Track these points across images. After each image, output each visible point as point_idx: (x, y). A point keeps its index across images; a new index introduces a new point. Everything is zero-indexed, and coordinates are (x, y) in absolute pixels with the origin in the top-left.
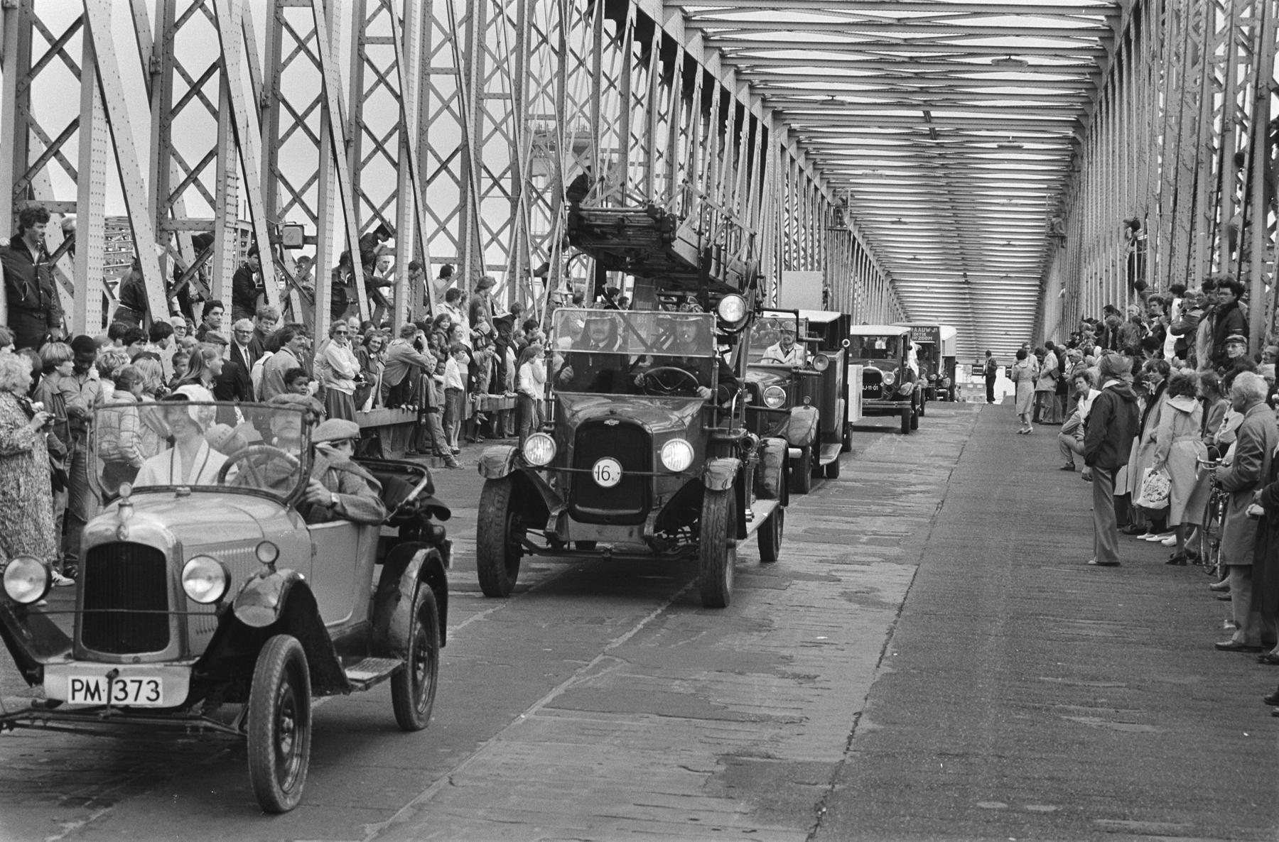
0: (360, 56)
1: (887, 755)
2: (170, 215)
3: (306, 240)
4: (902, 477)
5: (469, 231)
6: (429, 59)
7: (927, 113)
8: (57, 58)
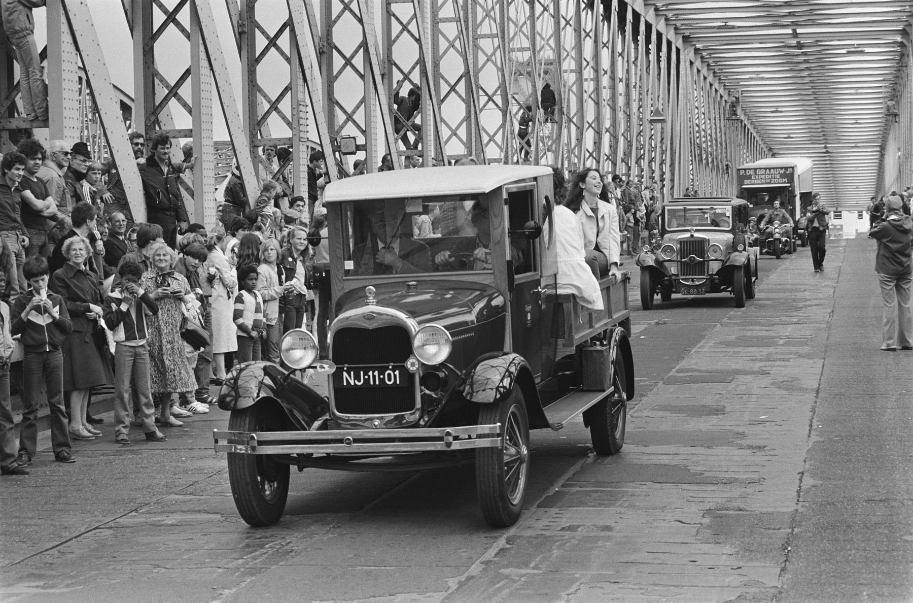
0: (388, 12)
1: (829, 504)
2: (259, 137)
3: (358, 148)
4: (800, 295)
5: (473, 135)
6: (438, 12)
7: (794, 30)
8: (172, 26)
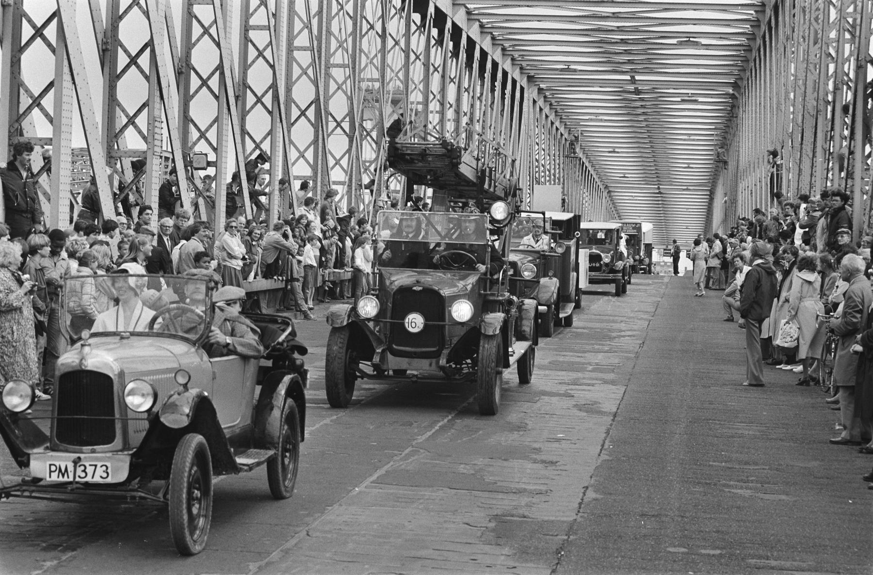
0: (246, 38)
1: (605, 516)
2: (116, 147)
3: (209, 164)
4: (616, 326)
5: (320, 158)
6: (293, 40)
7: (633, 77)
8: (39, 40)
